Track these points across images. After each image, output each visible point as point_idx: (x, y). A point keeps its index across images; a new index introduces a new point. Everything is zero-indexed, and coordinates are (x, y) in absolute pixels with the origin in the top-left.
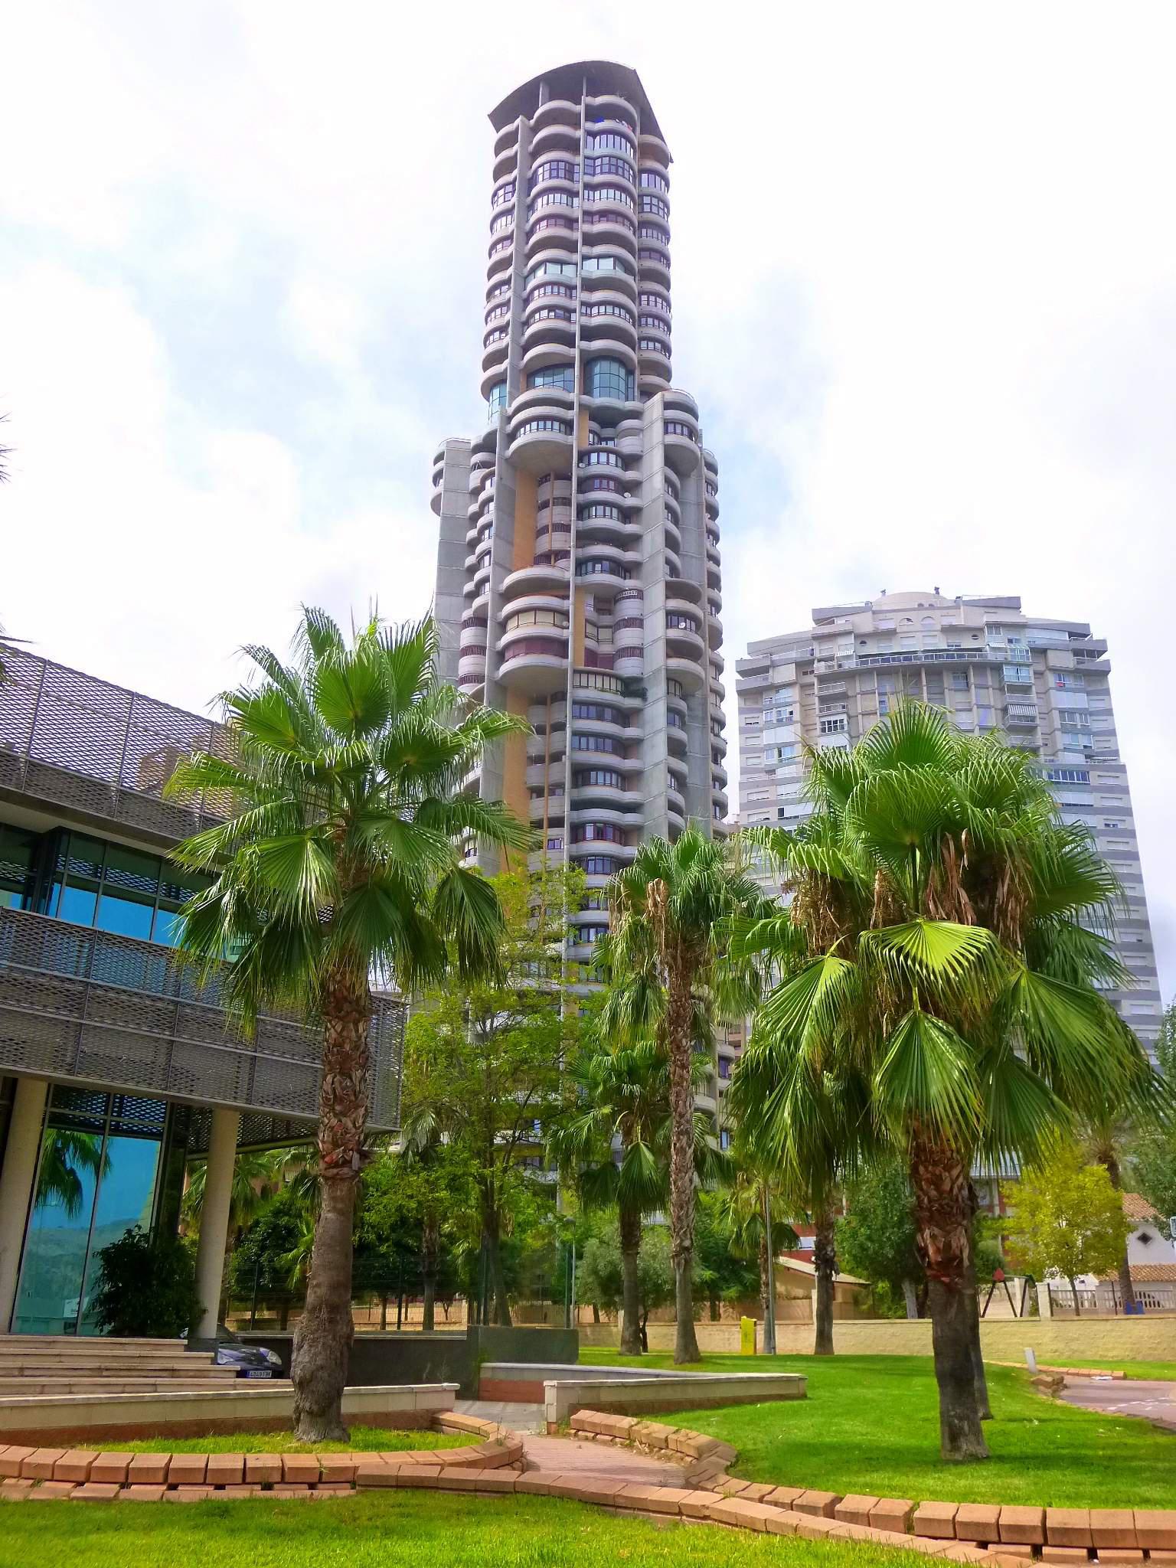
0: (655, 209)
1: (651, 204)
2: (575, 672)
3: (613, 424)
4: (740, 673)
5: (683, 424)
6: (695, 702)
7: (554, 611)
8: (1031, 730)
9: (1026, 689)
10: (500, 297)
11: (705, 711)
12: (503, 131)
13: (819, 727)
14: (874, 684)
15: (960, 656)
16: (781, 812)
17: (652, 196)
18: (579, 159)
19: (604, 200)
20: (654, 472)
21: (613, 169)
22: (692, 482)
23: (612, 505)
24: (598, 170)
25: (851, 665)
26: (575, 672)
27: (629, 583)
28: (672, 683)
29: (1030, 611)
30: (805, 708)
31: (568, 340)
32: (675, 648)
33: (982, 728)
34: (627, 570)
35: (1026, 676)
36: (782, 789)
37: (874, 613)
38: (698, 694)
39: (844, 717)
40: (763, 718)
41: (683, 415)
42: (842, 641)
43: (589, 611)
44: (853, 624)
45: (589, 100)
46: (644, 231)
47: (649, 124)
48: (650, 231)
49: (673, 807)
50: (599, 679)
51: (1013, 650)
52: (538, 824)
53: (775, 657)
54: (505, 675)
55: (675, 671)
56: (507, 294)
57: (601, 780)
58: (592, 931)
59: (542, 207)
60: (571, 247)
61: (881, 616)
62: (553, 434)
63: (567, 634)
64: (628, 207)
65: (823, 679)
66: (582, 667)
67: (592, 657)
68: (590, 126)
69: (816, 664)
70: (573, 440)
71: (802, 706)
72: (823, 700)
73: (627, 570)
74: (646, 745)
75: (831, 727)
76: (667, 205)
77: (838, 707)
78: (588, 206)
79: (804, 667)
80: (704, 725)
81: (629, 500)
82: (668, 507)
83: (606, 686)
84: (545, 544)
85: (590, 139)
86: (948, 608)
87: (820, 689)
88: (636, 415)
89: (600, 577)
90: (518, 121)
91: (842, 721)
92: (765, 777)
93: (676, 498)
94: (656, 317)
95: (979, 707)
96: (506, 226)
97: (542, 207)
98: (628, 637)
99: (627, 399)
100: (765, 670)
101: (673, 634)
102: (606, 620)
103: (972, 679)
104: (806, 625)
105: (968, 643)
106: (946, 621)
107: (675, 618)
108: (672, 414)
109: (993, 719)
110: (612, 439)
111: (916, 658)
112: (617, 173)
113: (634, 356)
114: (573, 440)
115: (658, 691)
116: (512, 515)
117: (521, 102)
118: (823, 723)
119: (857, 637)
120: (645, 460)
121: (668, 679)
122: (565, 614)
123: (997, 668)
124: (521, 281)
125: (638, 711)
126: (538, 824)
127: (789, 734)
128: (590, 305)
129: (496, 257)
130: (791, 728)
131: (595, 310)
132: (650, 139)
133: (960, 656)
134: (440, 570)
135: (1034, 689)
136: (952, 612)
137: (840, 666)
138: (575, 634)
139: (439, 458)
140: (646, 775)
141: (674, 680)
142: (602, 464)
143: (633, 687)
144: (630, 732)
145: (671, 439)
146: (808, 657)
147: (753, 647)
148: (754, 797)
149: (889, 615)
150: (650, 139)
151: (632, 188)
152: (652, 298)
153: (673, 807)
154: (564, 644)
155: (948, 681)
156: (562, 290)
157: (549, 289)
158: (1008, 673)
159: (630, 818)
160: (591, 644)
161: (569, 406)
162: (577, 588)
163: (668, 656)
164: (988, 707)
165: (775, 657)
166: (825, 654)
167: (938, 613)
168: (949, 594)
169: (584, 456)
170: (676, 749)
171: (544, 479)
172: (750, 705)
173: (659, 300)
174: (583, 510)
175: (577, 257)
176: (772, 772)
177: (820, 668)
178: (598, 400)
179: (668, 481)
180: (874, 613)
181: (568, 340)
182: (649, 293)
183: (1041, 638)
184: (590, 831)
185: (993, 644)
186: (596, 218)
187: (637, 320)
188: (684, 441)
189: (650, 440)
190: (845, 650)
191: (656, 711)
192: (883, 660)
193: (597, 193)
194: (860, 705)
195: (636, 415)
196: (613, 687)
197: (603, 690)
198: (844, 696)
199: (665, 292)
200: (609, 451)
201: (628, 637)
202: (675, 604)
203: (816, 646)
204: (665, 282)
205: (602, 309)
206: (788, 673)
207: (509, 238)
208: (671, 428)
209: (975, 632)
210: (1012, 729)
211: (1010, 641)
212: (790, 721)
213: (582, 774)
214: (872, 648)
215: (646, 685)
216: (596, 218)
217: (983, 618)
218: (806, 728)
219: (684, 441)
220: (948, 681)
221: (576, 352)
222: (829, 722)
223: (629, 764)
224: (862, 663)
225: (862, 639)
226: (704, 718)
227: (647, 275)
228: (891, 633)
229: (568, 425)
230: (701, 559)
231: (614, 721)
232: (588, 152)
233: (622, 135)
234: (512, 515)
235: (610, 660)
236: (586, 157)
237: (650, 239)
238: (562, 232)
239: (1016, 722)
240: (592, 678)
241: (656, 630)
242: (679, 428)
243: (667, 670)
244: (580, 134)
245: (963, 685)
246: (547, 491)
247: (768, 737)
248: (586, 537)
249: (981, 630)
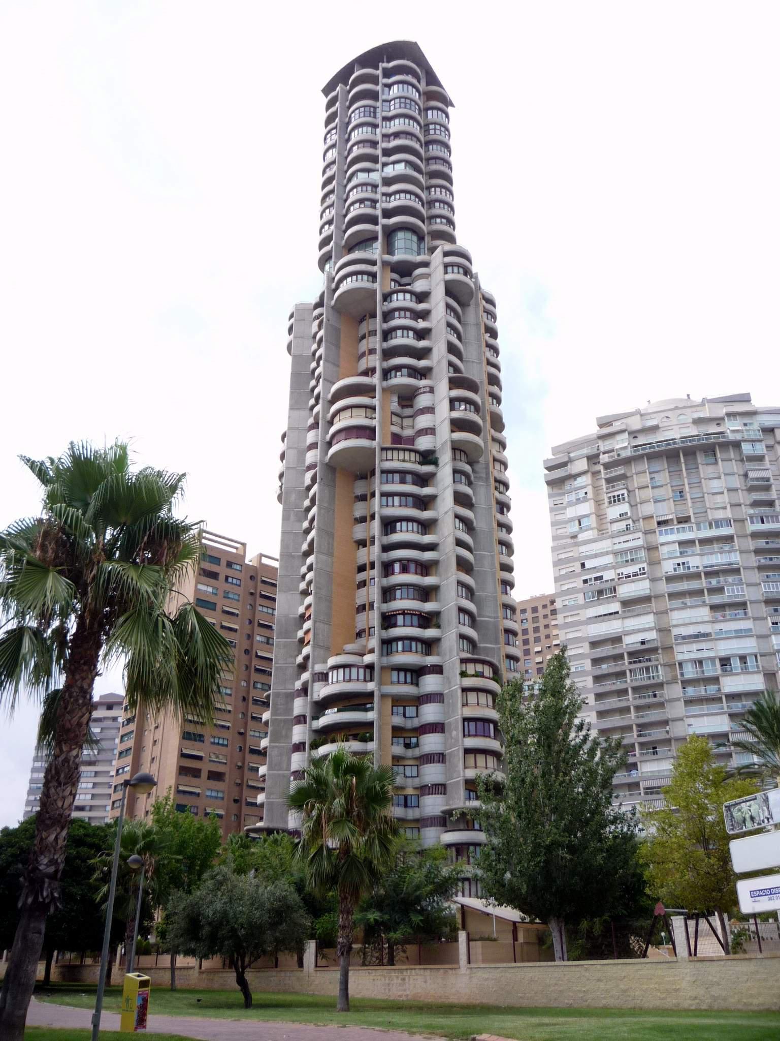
0: (438, 132)
1: (435, 129)
2: (382, 449)
3: (410, 275)
4: (546, 468)
5: (459, 266)
6: (478, 467)
7: (366, 407)
8: (768, 488)
9: (761, 458)
10: (328, 202)
11: (487, 474)
12: (330, 96)
13: (606, 500)
14: (645, 465)
15: (707, 439)
16: (583, 565)
17: (435, 124)
18: (379, 104)
19: (397, 125)
20: (438, 303)
21: (403, 105)
22: (471, 310)
23: (408, 328)
24: (392, 108)
25: (628, 453)
26: (382, 449)
27: (423, 383)
28: (458, 453)
29: (758, 403)
30: (596, 489)
31: (373, 220)
32: (457, 425)
33: (729, 490)
34: (423, 373)
35: (760, 449)
36: (583, 549)
37: (642, 415)
38: (482, 460)
39: (625, 491)
40: (566, 499)
41: (460, 260)
42: (619, 437)
43: (394, 406)
44: (626, 424)
45: (385, 65)
46: (431, 147)
47: (432, 79)
48: (435, 147)
49: (460, 543)
50: (401, 453)
51: (748, 431)
52: (361, 569)
53: (572, 455)
54: (331, 458)
55: (460, 441)
56: (333, 197)
57: (404, 528)
58: (400, 643)
59: (355, 136)
60: (375, 159)
61: (648, 417)
62: (363, 283)
63: (375, 423)
64: (416, 129)
65: (607, 466)
66: (389, 445)
67: (397, 438)
68: (386, 81)
69: (601, 456)
70: (377, 286)
71: (594, 487)
72: (609, 481)
73: (423, 373)
74: (439, 500)
75: (616, 500)
76: (447, 129)
77: (620, 484)
78: (385, 131)
79: (593, 459)
80: (488, 485)
81: (421, 324)
82: (449, 325)
83: (407, 458)
84: (363, 365)
85: (386, 89)
86: (697, 406)
87: (606, 474)
88: (426, 264)
89: (400, 379)
90: (338, 88)
91: (623, 495)
92: (569, 541)
93: (460, 322)
94: (441, 201)
95: (726, 474)
96: (332, 155)
97: (355, 136)
98: (423, 421)
99: (419, 254)
100: (564, 465)
101: (455, 414)
102: (408, 412)
103: (718, 455)
104: (594, 430)
105: (713, 429)
106: (696, 416)
107: (457, 404)
108: (449, 259)
109: (737, 482)
110: (409, 284)
111: (675, 443)
112: (405, 107)
113: (424, 227)
114: (377, 286)
115: (446, 458)
116: (338, 346)
117: (343, 76)
118: (610, 498)
119: (630, 433)
120: (433, 294)
121: (454, 449)
122: (373, 408)
123: (737, 445)
124: (342, 188)
125: (433, 475)
126: (361, 569)
127: (586, 508)
128: (389, 195)
129: (326, 176)
130: (587, 504)
131: (393, 198)
132: (433, 88)
133: (707, 439)
134: (292, 393)
135: (766, 457)
136: (699, 409)
137: (619, 455)
138: (382, 423)
139: (291, 316)
140: (439, 522)
141: (457, 448)
142: (401, 300)
143: (428, 457)
144: (427, 491)
145: (449, 277)
146: (595, 451)
147: (555, 450)
148: (563, 556)
149: (653, 416)
150: (433, 88)
151: (418, 117)
152: (438, 189)
153: (460, 543)
154: (373, 430)
155: (700, 458)
156: (369, 188)
157: (359, 189)
158: (746, 448)
159: (428, 555)
160: (396, 429)
161: (374, 263)
162: (384, 390)
163: (452, 431)
164: (733, 474)
165: (572, 455)
166: (607, 448)
167: (689, 410)
168: (697, 398)
169: (386, 297)
170: (461, 499)
171: (362, 320)
172: (556, 491)
173: (443, 190)
174: (388, 593)
175: (379, 166)
176: (574, 537)
177: (604, 458)
178: (399, 256)
179: (448, 306)
180: (642, 415)
181: (373, 220)
182: (436, 186)
183: (769, 421)
184: (397, 567)
185: (731, 428)
186: (392, 138)
187: (431, 203)
188: (461, 277)
189: (433, 281)
190: (621, 443)
191: (445, 472)
192: (650, 448)
193: (392, 122)
194: (636, 482)
195: (426, 264)
196: (413, 459)
197: (404, 461)
198: (624, 477)
199: (448, 185)
200: (405, 292)
201: (423, 421)
202: (456, 393)
203: (600, 443)
204: (449, 179)
205: (397, 196)
206: (582, 465)
207: (333, 163)
208: (450, 269)
209: (719, 421)
210: (751, 489)
211: (745, 425)
212: (585, 500)
213: (389, 525)
214: (642, 440)
215: (437, 455)
216: (392, 138)
217: (722, 411)
218: (598, 503)
219: (461, 277)
220: (700, 458)
221: (379, 228)
222: (614, 497)
223: (426, 515)
224: (635, 451)
225: (634, 434)
226: (487, 479)
227: (434, 175)
228: (655, 429)
229: (373, 276)
230: (481, 363)
231: (414, 483)
232: (385, 97)
233: (414, 86)
234: (338, 346)
235: (412, 440)
236: (384, 101)
237: (435, 150)
238: (368, 150)
239: (756, 483)
240: (395, 453)
241: (443, 413)
242: (456, 269)
243: (453, 442)
244: (379, 88)
245: (713, 460)
246: (364, 328)
247: (571, 512)
248: (388, 354)
249: (723, 419)
